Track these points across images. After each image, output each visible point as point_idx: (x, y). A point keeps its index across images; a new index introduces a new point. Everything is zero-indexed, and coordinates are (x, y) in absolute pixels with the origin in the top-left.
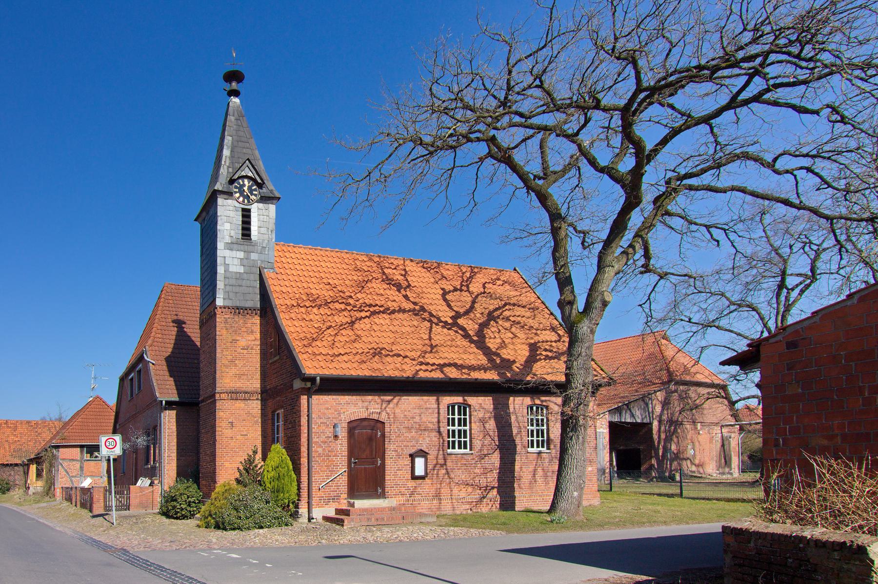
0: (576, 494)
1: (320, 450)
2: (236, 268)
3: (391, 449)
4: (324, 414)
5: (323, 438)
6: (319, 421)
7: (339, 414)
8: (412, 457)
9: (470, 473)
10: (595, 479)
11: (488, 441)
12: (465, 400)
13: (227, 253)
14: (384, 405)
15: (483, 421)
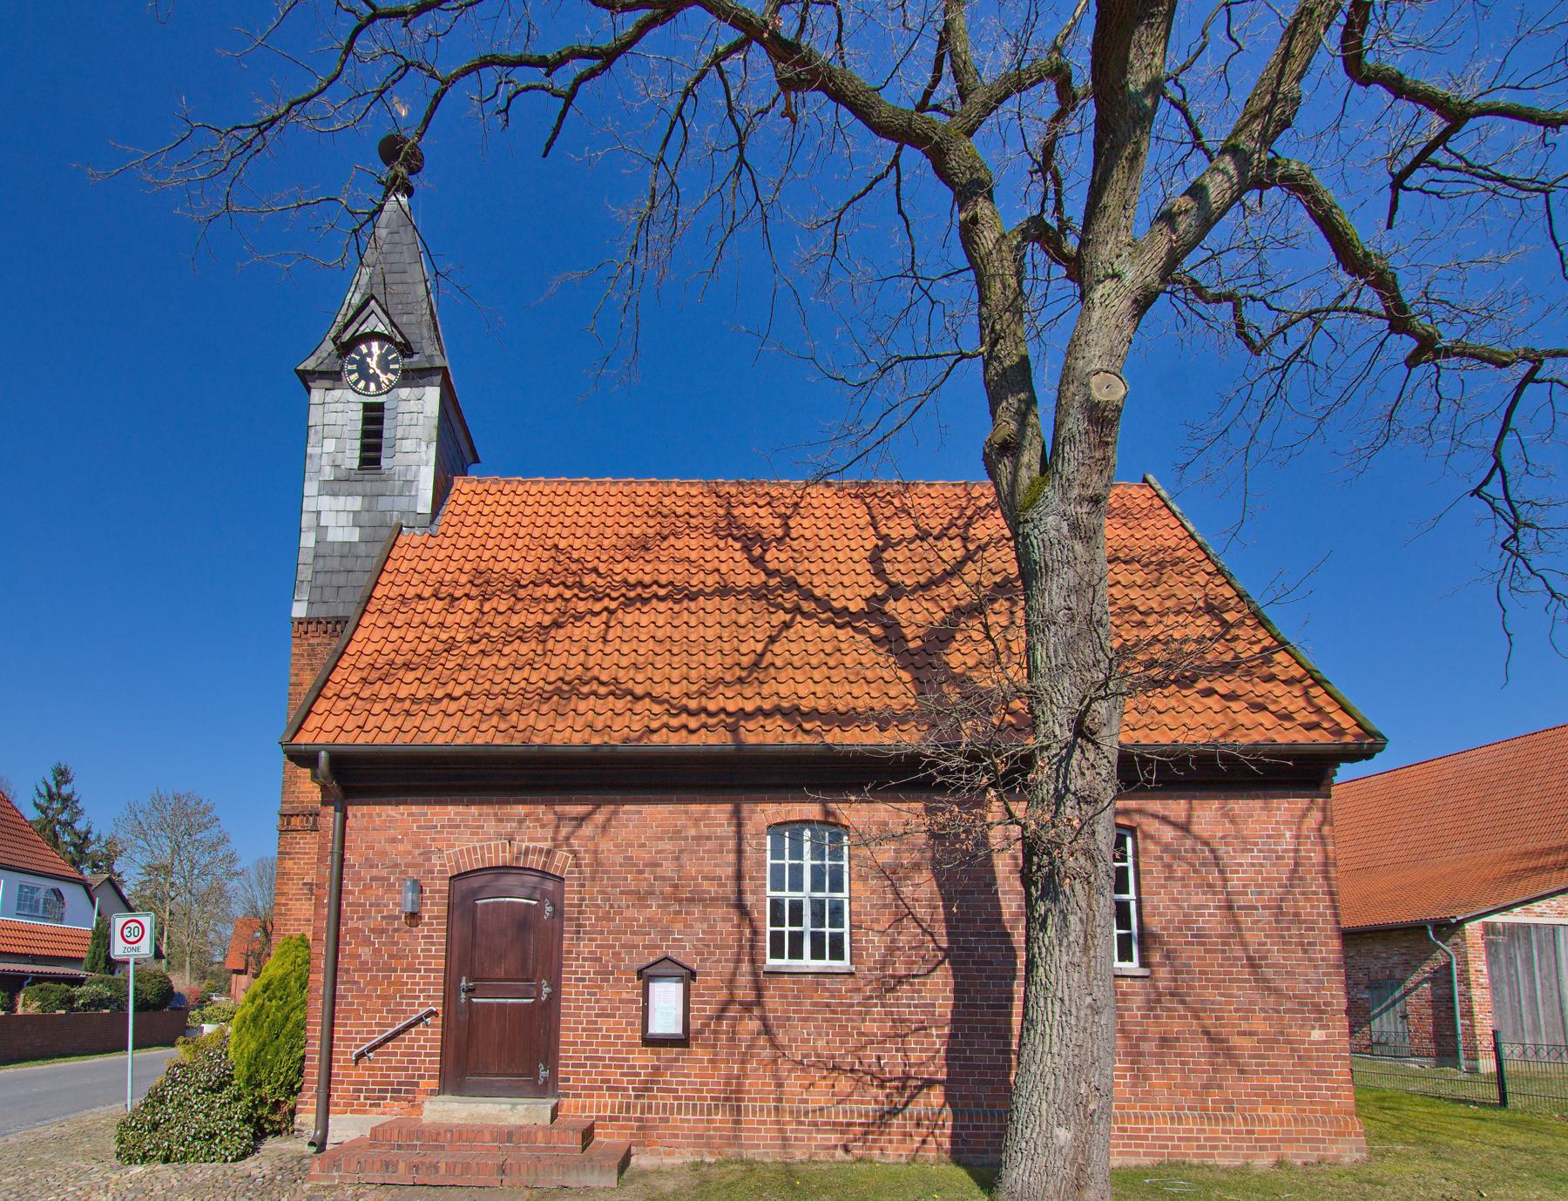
0: (1063, 1135)
1: (366, 953)
2: (342, 532)
3: (580, 957)
4: (384, 853)
5: (377, 919)
6: (368, 874)
7: (427, 855)
8: (646, 976)
9: (844, 1033)
10: (1340, 1071)
12: (827, 813)
13: (326, 502)
14: (564, 831)
15: (891, 875)
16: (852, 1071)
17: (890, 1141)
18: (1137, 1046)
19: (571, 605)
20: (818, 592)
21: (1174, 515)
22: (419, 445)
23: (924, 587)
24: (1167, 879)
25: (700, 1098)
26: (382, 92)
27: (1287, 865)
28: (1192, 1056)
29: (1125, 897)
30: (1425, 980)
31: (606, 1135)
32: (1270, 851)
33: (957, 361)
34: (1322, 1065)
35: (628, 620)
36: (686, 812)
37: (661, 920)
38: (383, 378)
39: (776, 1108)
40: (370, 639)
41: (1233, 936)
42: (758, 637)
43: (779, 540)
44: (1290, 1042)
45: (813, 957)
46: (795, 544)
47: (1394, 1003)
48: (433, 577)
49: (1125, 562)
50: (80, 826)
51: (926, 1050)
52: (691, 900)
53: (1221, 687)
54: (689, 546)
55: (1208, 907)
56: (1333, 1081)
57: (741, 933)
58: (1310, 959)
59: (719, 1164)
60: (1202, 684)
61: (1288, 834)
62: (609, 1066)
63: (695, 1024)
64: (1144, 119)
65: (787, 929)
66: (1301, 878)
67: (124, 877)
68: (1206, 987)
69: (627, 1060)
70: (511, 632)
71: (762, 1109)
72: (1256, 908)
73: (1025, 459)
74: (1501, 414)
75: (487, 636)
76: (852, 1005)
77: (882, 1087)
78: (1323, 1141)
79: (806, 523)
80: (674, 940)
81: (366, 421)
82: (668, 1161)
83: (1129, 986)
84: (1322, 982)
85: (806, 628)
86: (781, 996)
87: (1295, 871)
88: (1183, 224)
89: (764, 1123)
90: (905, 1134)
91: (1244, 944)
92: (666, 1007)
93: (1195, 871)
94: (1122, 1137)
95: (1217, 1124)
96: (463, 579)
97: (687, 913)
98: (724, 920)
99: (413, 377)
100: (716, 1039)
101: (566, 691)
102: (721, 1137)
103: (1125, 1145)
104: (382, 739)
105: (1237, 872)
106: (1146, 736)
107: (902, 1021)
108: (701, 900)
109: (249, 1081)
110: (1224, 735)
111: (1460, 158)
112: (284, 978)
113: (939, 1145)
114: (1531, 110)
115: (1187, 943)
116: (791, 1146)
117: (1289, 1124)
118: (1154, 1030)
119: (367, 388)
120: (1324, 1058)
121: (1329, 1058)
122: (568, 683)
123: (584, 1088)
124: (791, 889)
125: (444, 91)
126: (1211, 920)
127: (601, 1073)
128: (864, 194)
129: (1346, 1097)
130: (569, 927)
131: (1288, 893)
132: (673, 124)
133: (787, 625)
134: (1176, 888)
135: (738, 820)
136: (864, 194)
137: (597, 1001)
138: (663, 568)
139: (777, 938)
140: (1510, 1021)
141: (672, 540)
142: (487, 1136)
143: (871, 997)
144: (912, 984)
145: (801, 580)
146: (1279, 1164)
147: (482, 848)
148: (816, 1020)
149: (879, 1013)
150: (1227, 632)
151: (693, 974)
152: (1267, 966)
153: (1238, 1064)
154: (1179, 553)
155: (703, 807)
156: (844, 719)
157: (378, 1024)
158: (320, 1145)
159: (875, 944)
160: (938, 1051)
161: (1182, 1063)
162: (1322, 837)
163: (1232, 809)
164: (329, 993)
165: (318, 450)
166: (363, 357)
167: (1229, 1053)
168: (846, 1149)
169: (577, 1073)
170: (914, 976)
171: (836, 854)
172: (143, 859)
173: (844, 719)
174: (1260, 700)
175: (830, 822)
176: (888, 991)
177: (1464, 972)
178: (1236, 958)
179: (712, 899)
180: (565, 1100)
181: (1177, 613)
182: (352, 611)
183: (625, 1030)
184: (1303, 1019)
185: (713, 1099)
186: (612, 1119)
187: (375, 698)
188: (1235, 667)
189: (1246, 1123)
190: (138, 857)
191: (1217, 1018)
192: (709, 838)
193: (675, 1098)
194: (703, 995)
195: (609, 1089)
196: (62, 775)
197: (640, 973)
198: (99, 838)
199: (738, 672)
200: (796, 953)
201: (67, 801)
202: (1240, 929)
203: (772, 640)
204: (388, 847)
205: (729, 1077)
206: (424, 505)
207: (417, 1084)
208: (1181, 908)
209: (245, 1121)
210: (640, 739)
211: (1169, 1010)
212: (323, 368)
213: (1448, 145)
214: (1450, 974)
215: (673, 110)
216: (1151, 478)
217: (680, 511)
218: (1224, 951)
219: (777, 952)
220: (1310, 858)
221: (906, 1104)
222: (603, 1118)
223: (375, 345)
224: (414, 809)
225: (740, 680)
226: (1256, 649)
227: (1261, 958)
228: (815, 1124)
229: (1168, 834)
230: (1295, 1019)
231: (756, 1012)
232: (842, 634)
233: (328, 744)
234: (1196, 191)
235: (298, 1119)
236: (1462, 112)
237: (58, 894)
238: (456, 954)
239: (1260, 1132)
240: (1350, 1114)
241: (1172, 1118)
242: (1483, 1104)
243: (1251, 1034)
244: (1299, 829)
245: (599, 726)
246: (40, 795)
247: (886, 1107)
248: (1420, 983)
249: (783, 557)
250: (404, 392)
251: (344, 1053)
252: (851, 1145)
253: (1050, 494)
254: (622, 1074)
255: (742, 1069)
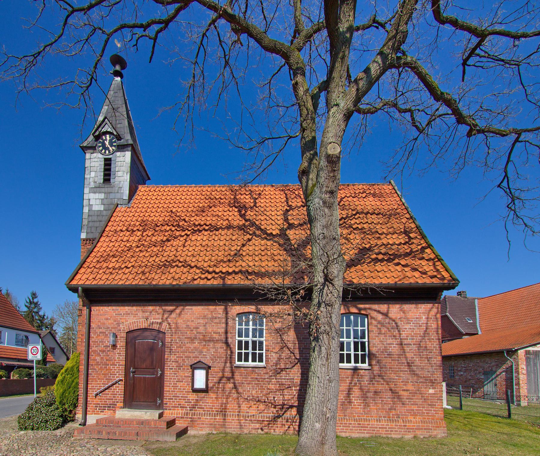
0: (318, 425)
1: (98, 358)
2: (98, 207)
3: (171, 361)
4: (104, 324)
5: (102, 347)
6: (99, 331)
7: (118, 324)
8: (194, 367)
9: (262, 389)
11: (286, 353)
13: (92, 196)
14: (166, 316)
16: (265, 402)
17: (277, 427)
18: (366, 394)
19: (174, 233)
20: (262, 227)
21: (398, 196)
22: (124, 174)
23: (301, 225)
24: (378, 334)
25: (212, 411)
26: (87, 40)
27: (423, 329)
28: (385, 398)
29: (364, 340)
30: (503, 371)
31: (180, 423)
32: (417, 323)
33: (288, 139)
34: (433, 402)
35: (193, 239)
36: (208, 309)
37: (199, 348)
38: (110, 148)
39: (238, 415)
40: (103, 246)
41: (402, 355)
42: (239, 244)
43: (251, 208)
44: (421, 394)
45: (252, 361)
46: (257, 209)
47: (492, 380)
48: (127, 223)
49: (377, 215)
50: (41, 313)
51: (291, 395)
52: (209, 341)
53: (403, 262)
54: (219, 210)
55: (393, 344)
56: (436, 408)
57: (227, 353)
58: (430, 363)
59: (217, 434)
60: (397, 261)
61: (424, 317)
62: (180, 399)
63: (210, 385)
64: (348, 42)
65: (243, 351)
66: (428, 334)
67: (57, 332)
68: (391, 373)
69: (187, 397)
70: (152, 243)
71: (233, 415)
72: (411, 345)
73: (311, 177)
74: (507, 154)
75: (143, 245)
76: (265, 379)
77: (275, 408)
78: (431, 429)
79: (262, 201)
80: (203, 355)
81: (105, 165)
82: (201, 432)
83: (363, 373)
84: (434, 372)
85: (256, 241)
86: (240, 375)
87: (426, 331)
88: (361, 84)
89: (234, 420)
90: (282, 424)
91: (406, 358)
92: (200, 379)
93: (389, 331)
94: (359, 427)
95: (393, 423)
96: (138, 224)
97: (208, 345)
98: (221, 348)
99: (121, 148)
100: (218, 390)
101: (167, 265)
102: (219, 425)
103: (360, 430)
104: (101, 283)
105: (404, 331)
106: (371, 281)
107: (282, 384)
108: (213, 341)
109: (60, 403)
110: (400, 280)
111: (486, 52)
112: (72, 367)
113: (294, 429)
114: (509, 32)
115: (385, 357)
116: (243, 428)
117: (419, 423)
118: (372, 389)
119: (105, 152)
120: (433, 399)
121: (435, 399)
122: (169, 262)
123: (172, 407)
124: (346, 338)
125: (109, 39)
126: (395, 349)
127: (178, 402)
128: (277, 73)
129: (441, 414)
130: (167, 350)
131: (423, 339)
132: (200, 48)
133: (249, 240)
134: (382, 337)
135: (226, 312)
136: (277, 73)
137: (177, 376)
138: (209, 219)
139: (240, 354)
140: (533, 387)
141: (213, 208)
142: (135, 423)
143: (272, 376)
144: (286, 371)
145: (257, 223)
146: (415, 437)
147: (137, 322)
148: (252, 384)
149: (274, 382)
150: (410, 241)
151: (209, 367)
152: (414, 366)
153: (402, 401)
154: (398, 211)
155: (214, 307)
156: (261, 275)
157: (103, 384)
158: (84, 424)
159: (274, 357)
160: (295, 395)
161: (382, 401)
162: (437, 318)
163: (404, 308)
164: (86, 372)
165: (88, 176)
166: (104, 141)
167: (399, 397)
168: (262, 429)
169: (169, 401)
170: (287, 368)
171: (261, 325)
172: (63, 325)
173: (261, 275)
174: (417, 267)
175: (257, 312)
176: (278, 374)
177: (517, 368)
178: (403, 363)
179: (216, 340)
180: (166, 411)
181: (393, 234)
182: (97, 235)
183: (186, 387)
184: (426, 385)
185: (216, 411)
186: (182, 418)
187: (100, 269)
188: (410, 255)
189: (403, 423)
190: (61, 325)
191: (395, 385)
192: (216, 318)
193: (203, 411)
194: (213, 375)
195: (181, 407)
196: (34, 295)
197: (191, 366)
198: (47, 318)
199: (229, 257)
200: (349, 361)
201: (36, 304)
202: (404, 352)
203: (243, 245)
204: (105, 321)
205: (222, 404)
206: (126, 197)
207: (116, 405)
208: (383, 344)
209: (60, 416)
210: (189, 282)
211: (378, 381)
212: (89, 145)
213: (481, 47)
214: (512, 369)
215: (199, 43)
216: (392, 182)
217: (217, 197)
218: (398, 360)
219: (240, 360)
220: (431, 326)
221: (283, 414)
222: (179, 417)
223: (108, 136)
224: (114, 308)
225: (229, 261)
226: (419, 247)
227: (412, 363)
228: (251, 420)
229: (380, 317)
230: (423, 385)
231: (232, 381)
232: (269, 243)
233: (82, 285)
234: (367, 71)
235: (77, 416)
236: (482, 34)
237: (27, 337)
238: (129, 360)
239: (409, 426)
240: (442, 420)
241: (377, 420)
242: (503, 417)
243: (407, 390)
244: (428, 315)
245: (176, 277)
246: (27, 302)
247: (276, 415)
248: (501, 372)
249: (252, 214)
250: (118, 154)
251: (92, 394)
252: (264, 428)
253: (316, 190)
254: (185, 402)
255: (227, 401)
